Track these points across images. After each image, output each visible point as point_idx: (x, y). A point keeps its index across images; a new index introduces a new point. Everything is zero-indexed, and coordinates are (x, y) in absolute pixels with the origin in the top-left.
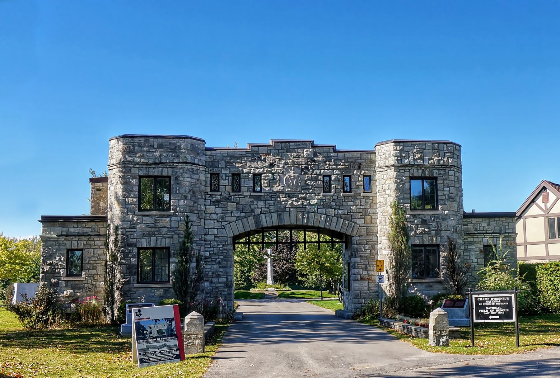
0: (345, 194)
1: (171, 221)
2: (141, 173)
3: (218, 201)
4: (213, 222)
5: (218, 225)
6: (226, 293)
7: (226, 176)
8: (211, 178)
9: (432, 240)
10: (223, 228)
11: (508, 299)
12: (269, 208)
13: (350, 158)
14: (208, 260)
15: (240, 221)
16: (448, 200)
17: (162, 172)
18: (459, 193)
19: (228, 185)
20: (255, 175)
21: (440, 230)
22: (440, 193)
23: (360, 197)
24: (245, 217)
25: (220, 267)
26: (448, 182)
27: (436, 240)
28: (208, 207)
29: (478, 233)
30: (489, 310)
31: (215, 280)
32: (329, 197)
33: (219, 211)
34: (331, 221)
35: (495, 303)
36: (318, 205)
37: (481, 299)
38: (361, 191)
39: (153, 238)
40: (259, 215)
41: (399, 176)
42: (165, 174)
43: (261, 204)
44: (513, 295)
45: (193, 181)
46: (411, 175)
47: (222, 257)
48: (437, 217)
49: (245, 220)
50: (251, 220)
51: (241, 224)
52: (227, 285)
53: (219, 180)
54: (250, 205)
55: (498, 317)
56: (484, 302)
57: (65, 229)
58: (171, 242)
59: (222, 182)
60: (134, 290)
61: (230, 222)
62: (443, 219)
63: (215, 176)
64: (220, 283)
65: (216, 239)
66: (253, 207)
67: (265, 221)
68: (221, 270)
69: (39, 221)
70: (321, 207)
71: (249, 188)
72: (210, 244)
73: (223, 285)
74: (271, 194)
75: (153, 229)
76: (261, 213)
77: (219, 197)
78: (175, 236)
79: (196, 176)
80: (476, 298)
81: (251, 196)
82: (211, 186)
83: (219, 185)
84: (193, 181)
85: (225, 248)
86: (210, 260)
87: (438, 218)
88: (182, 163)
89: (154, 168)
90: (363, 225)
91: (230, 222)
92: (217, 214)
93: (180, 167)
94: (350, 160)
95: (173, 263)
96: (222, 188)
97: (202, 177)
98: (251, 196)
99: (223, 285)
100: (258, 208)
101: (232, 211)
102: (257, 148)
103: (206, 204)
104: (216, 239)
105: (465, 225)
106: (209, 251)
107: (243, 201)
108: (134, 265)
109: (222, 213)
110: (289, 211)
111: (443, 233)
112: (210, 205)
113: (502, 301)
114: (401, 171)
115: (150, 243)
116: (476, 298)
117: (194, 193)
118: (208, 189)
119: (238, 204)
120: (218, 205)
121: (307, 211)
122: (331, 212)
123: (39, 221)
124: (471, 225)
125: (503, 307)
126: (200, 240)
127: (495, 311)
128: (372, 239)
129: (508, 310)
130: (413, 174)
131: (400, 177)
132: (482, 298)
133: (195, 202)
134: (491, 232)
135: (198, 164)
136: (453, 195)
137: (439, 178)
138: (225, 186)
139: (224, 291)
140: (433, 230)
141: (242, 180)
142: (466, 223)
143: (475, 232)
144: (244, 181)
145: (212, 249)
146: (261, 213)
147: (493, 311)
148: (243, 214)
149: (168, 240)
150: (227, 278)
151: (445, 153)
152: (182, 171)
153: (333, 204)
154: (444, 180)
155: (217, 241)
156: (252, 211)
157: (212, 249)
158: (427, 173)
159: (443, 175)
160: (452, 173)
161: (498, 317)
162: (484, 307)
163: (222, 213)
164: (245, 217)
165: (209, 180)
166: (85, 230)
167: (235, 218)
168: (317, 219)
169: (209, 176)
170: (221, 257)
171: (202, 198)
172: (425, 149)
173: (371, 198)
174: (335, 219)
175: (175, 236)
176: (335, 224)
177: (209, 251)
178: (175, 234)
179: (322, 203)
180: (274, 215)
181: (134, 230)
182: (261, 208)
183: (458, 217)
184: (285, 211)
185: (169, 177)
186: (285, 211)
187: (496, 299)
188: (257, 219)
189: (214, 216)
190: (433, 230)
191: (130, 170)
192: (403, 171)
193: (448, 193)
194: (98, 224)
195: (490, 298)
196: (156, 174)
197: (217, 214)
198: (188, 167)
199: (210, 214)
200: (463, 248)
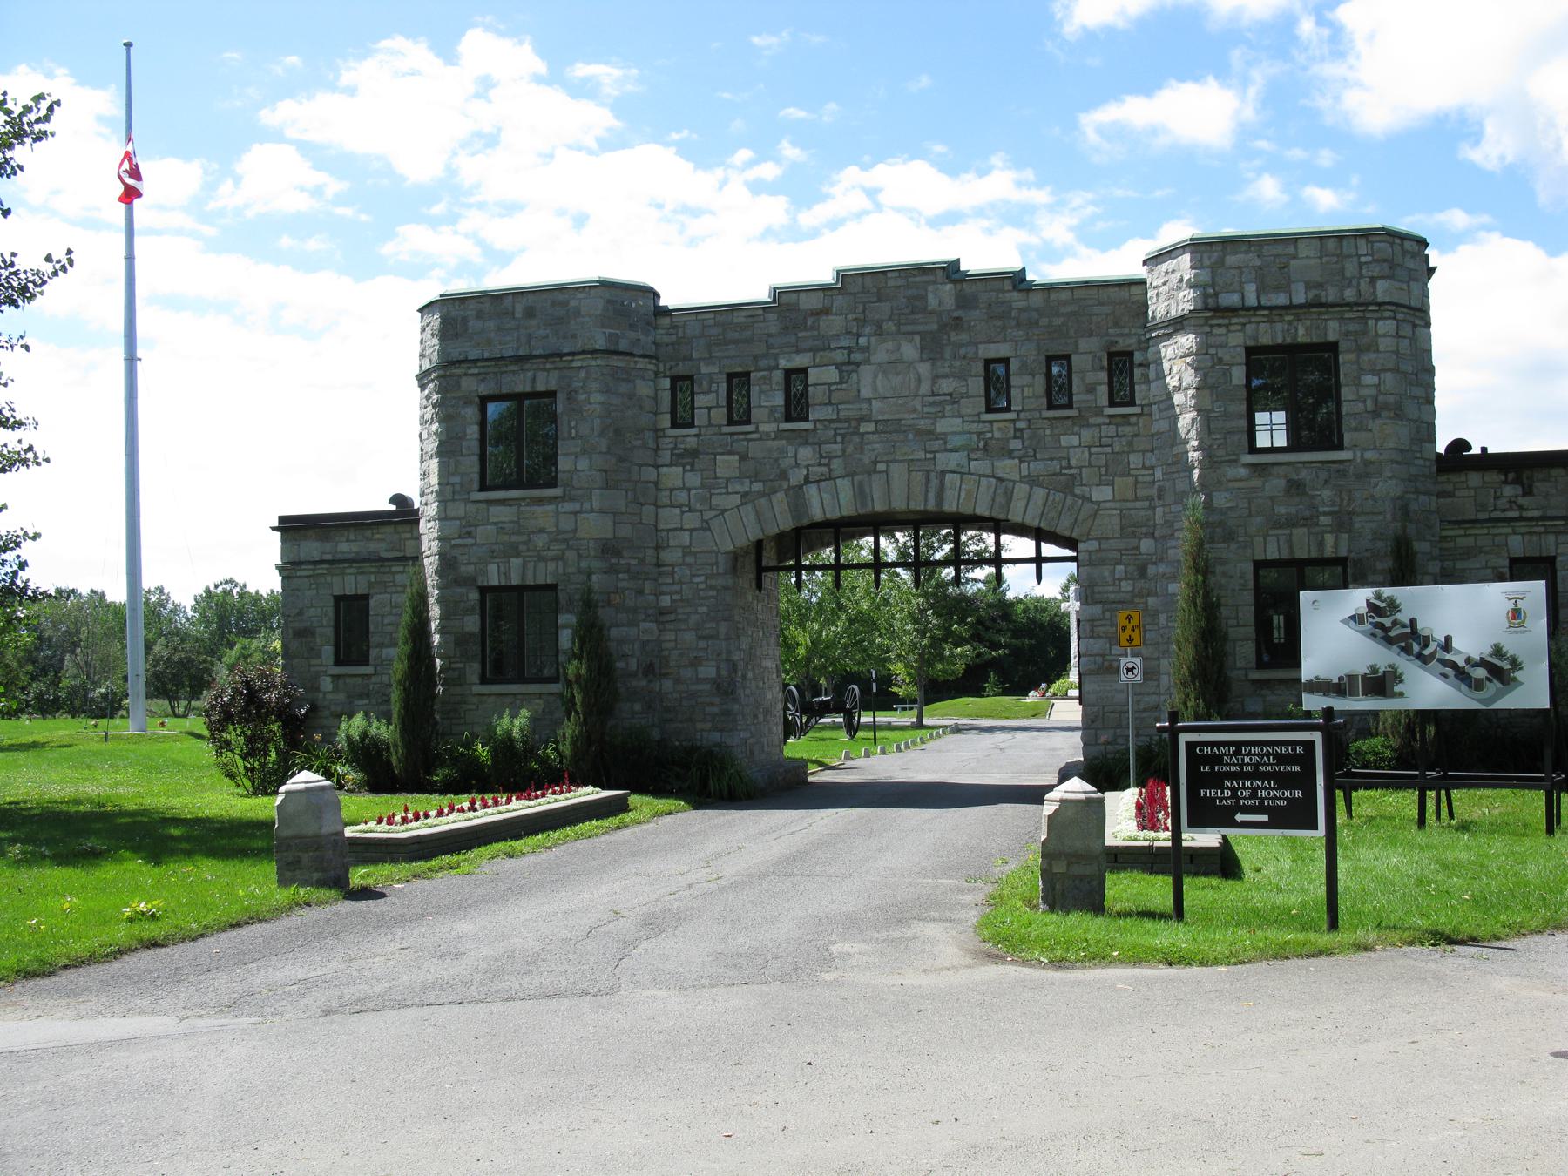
0: (1052, 414)
1: (557, 513)
2: (484, 389)
3: (694, 453)
4: (677, 511)
5: (691, 520)
6: (716, 710)
7: (711, 382)
8: (673, 389)
9: (1321, 544)
10: (706, 527)
11: (1300, 750)
12: (828, 465)
13: (1065, 303)
14: (668, 618)
15: (749, 507)
16: (1376, 414)
17: (534, 380)
18: (1419, 392)
19: (718, 406)
20: (788, 373)
21: (1351, 514)
22: (1346, 393)
23: (1099, 420)
24: (763, 494)
25: (700, 638)
26: (1373, 356)
27: (1336, 545)
28: (664, 470)
29: (1490, 520)
30: (1234, 790)
31: (687, 673)
32: (1001, 425)
33: (694, 479)
34: (1009, 496)
35: (1257, 765)
36: (973, 450)
37: (1208, 750)
38: (1103, 399)
39: (516, 562)
40: (800, 487)
41: (1209, 346)
42: (541, 387)
43: (806, 454)
44: (1317, 737)
45: (615, 401)
46: (1251, 343)
47: (705, 609)
48: (1340, 469)
49: (763, 501)
50: (780, 501)
51: (752, 516)
52: (718, 688)
53: (693, 394)
54: (777, 460)
55: (1265, 818)
56: (1218, 759)
57: (328, 546)
58: (561, 571)
59: (700, 400)
60: (475, 700)
61: (724, 511)
62: (1359, 477)
63: (683, 384)
64: (699, 681)
65: (689, 560)
66: (785, 463)
67: (820, 505)
68: (702, 644)
69: (274, 529)
70: (979, 454)
71: (772, 410)
72: (673, 573)
73: (707, 687)
74: (834, 425)
75: (514, 539)
76: (807, 481)
77: (692, 443)
78: (568, 554)
79: (624, 388)
80: (1190, 746)
81: (780, 434)
82: (673, 412)
83: (693, 408)
84: (615, 401)
85: (713, 582)
86: (673, 617)
87: (1343, 474)
88: (583, 352)
89: (514, 373)
90: (1108, 505)
91: (724, 511)
92: (689, 490)
93: (579, 364)
94: (1069, 309)
95: (565, 626)
96: (700, 417)
97: (644, 389)
98: (780, 434)
99: (707, 687)
100: (797, 465)
101: (728, 480)
102: (794, 296)
103: (660, 461)
104: (689, 560)
105: (1440, 495)
106: (671, 594)
107: (755, 450)
108: (471, 635)
109: (703, 486)
110: (886, 472)
111: (1359, 523)
112: (671, 465)
113: (1281, 759)
114: (1216, 331)
115: (507, 575)
116: (1190, 746)
117: (617, 432)
118: (666, 421)
119: (744, 457)
120: (692, 465)
121: (939, 468)
122: (1006, 467)
123: (274, 529)
124: (1465, 493)
125: (1283, 781)
126: (642, 561)
127: (1254, 795)
128: (1138, 548)
129: (1298, 794)
130: (1255, 338)
131: (1212, 351)
132: (1212, 744)
133: (621, 460)
134: (1536, 513)
135: (631, 354)
136: (1391, 399)
137: (1342, 346)
138: (709, 409)
139: (712, 704)
140: (1325, 514)
141: (755, 390)
142: (1449, 488)
143: (1481, 516)
144: (761, 392)
145: (677, 587)
146: (807, 481)
147: (1246, 793)
148: (757, 487)
149: (551, 566)
150: (718, 668)
151: (1361, 265)
152: (582, 374)
153: (1015, 444)
154: (1360, 350)
155: (689, 565)
156: (783, 475)
157: (677, 587)
158: (1301, 331)
159: (1356, 333)
160: (1387, 326)
161: (1265, 818)
162: (1217, 781)
163: (703, 486)
164: (763, 494)
165: (666, 397)
166: (372, 546)
167: (737, 499)
168: (969, 492)
169: (667, 383)
170: (701, 610)
171: (645, 446)
172: (1295, 257)
173: (1133, 420)
174: (1021, 490)
175: (568, 554)
176: (1022, 504)
177: (671, 594)
178: (569, 548)
179: (982, 444)
180: (844, 485)
181: (470, 541)
182: (807, 467)
183: (1413, 470)
184: (875, 471)
185: (551, 394)
186: (875, 471)
187: (1258, 750)
188: (797, 500)
189: (682, 497)
190: (1325, 514)
191: (458, 383)
192: (1223, 330)
193: (1373, 392)
194: (400, 528)
195: (1238, 744)
196: (519, 389)
197: (689, 490)
198: (599, 362)
199: (672, 490)
200: (1437, 570)
